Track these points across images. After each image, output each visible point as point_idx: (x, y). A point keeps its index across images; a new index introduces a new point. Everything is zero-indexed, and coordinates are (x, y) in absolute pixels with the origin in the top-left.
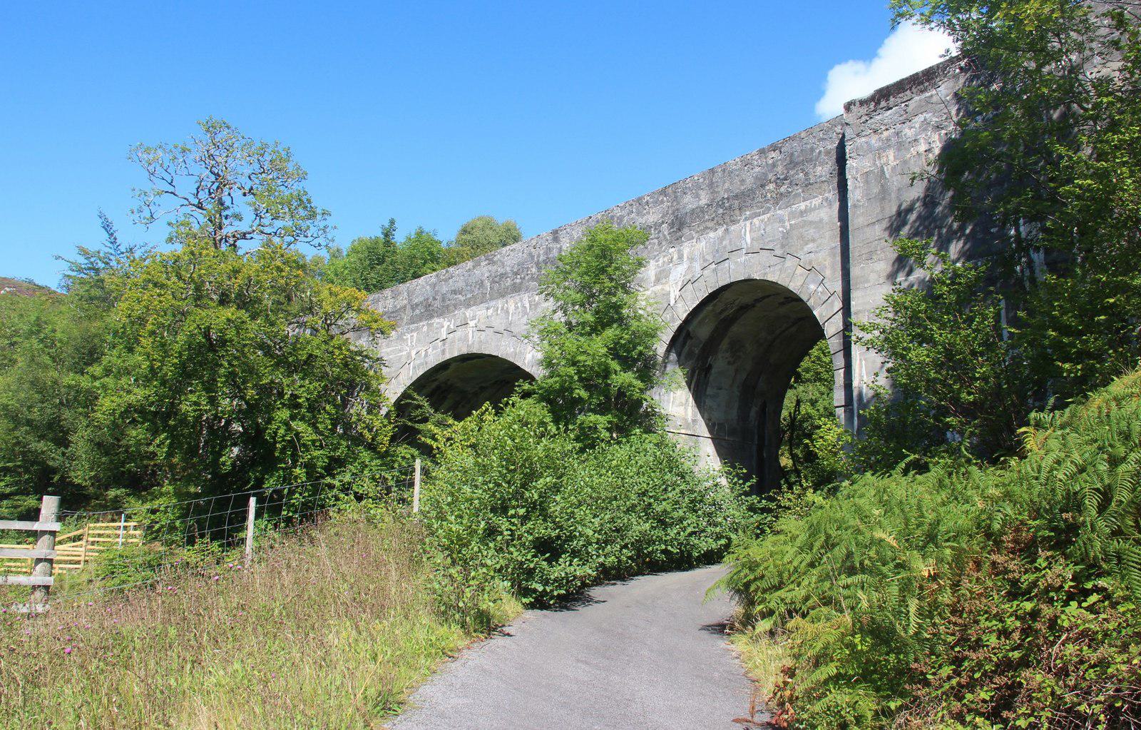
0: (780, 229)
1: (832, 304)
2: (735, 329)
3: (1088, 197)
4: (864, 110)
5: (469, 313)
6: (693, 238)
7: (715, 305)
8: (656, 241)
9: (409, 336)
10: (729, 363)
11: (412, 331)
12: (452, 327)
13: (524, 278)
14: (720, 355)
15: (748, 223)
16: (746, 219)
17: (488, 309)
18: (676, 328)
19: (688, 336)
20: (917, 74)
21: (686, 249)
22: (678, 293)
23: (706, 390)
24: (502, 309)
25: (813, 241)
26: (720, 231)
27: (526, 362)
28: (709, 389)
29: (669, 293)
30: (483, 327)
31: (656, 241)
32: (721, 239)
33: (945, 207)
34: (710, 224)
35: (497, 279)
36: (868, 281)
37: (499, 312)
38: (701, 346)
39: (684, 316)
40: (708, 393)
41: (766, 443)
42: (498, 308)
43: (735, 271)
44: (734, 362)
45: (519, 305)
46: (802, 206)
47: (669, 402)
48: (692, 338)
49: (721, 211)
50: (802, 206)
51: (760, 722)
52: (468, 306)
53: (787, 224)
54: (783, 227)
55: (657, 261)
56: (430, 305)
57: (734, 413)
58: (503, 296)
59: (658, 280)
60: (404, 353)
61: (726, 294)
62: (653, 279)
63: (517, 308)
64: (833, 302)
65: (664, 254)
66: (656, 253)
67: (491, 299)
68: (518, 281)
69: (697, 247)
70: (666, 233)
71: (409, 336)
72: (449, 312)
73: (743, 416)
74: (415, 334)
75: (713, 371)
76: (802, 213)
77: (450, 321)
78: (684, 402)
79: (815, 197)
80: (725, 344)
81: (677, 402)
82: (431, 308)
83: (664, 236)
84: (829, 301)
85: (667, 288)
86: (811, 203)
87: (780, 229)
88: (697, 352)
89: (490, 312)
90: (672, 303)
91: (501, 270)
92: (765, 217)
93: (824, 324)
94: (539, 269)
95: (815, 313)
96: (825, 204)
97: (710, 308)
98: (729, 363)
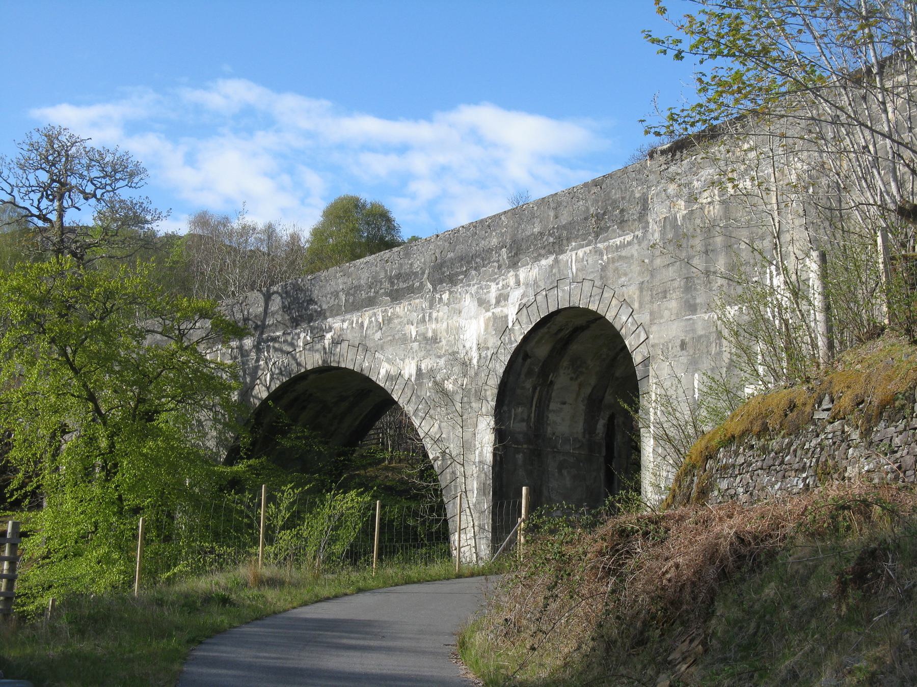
0: (600, 262)
1: (639, 336)
4: (662, 159)
6: (528, 264)
7: (549, 328)
8: (496, 264)
10: (571, 379)
13: (378, 292)
14: (561, 372)
15: (574, 253)
16: (572, 250)
17: (343, 321)
18: (513, 349)
19: (526, 356)
21: (523, 273)
23: (548, 406)
24: (357, 322)
25: (626, 275)
26: (552, 258)
27: (380, 377)
29: (506, 316)
31: (496, 264)
32: (552, 267)
33: (231, 472)
34: (543, 252)
36: (662, 317)
37: (354, 325)
38: (540, 364)
39: (520, 338)
40: (551, 408)
41: (616, 454)
42: (353, 322)
43: (562, 299)
44: (576, 379)
45: (373, 319)
46: (618, 241)
47: (510, 418)
48: (530, 357)
50: (618, 241)
53: (605, 257)
54: (602, 260)
55: (497, 284)
57: (580, 427)
58: (358, 310)
59: (498, 302)
61: (559, 319)
62: (493, 301)
63: (370, 322)
64: (640, 332)
65: (504, 277)
66: (496, 276)
67: (346, 312)
69: (529, 272)
70: (505, 257)
73: (590, 429)
75: (555, 387)
76: (617, 248)
78: (526, 418)
79: (627, 234)
83: (503, 259)
84: (637, 332)
85: (505, 310)
86: (624, 239)
87: (600, 262)
88: (536, 370)
90: (510, 325)
92: (587, 249)
93: (632, 352)
94: (392, 284)
95: (627, 343)
96: (635, 241)
98: (571, 379)
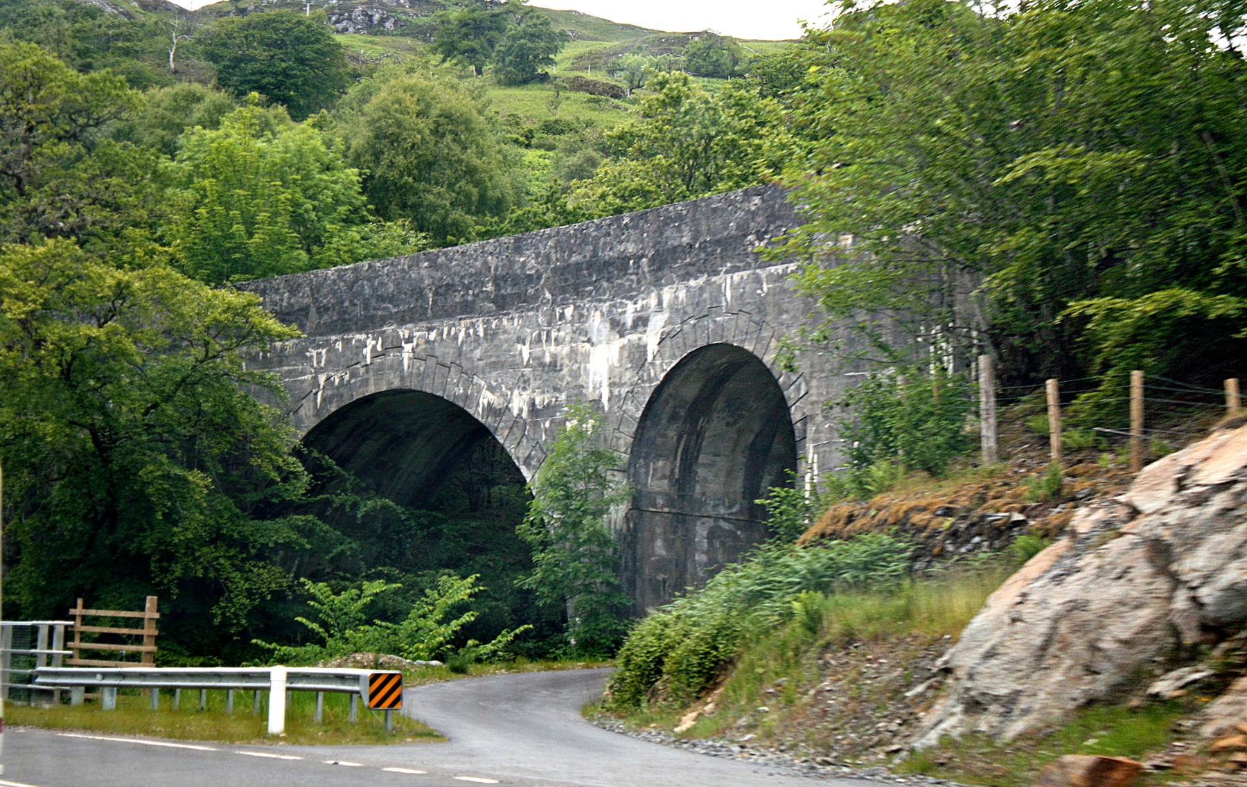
2: (730, 386)
3: (669, 545)
5: (404, 332)
9: (314, 353)
10: (728, 424)
11: (319, 346)
12: (379, 348)
14: (715, 415)
15: (729, 276)
16: (726, 272)
20: (267, 720)
22: (656, 348)
26: (701, 280)
28: (701, 456)
30: (423, 355)
35: (441, 291)
44: (734, 424)
45: (471, 331)
49: (703, 255)
51: (1096, 705)
52: (402, 321)
56: (345, 312)
60: (309, 377)
63: (468, 335)
68: (470, 298)
71: (314, 353)
72: (374, 327)
74: (324, 351)
77: (376, 339)
80: (720, 403)
81: (659, 475)
82: (347, 317)
89: (433, 336)
91: (447, 280)
94: (497, 286)
97: (693, 365)
98: (728, 424)
